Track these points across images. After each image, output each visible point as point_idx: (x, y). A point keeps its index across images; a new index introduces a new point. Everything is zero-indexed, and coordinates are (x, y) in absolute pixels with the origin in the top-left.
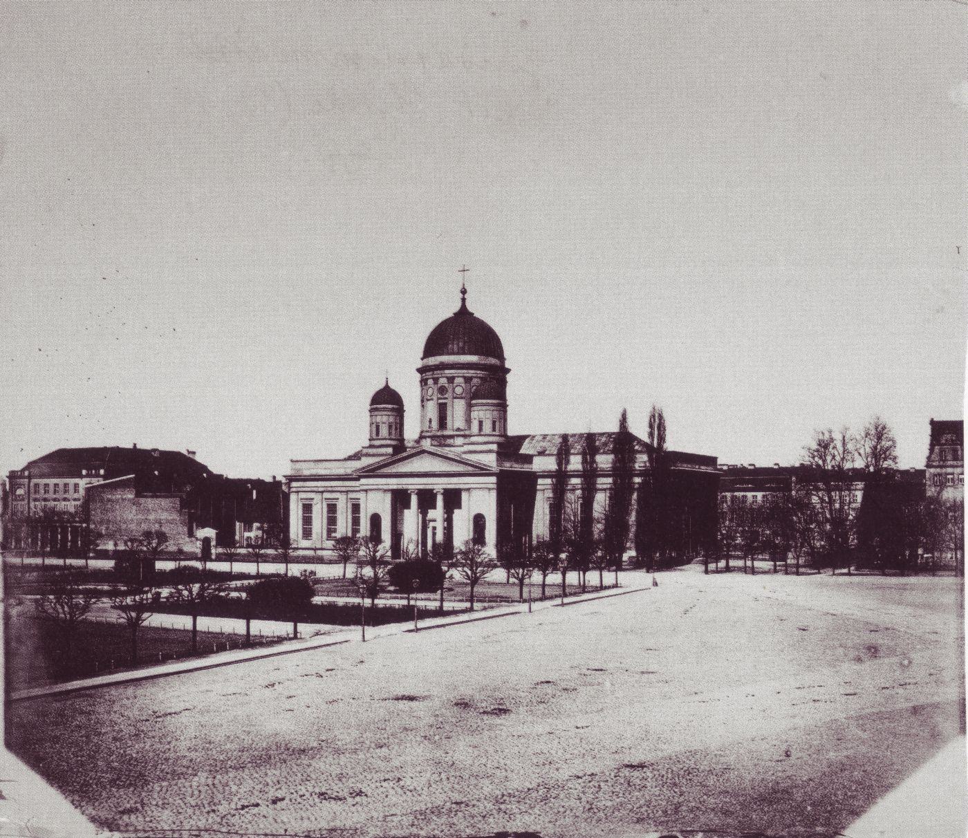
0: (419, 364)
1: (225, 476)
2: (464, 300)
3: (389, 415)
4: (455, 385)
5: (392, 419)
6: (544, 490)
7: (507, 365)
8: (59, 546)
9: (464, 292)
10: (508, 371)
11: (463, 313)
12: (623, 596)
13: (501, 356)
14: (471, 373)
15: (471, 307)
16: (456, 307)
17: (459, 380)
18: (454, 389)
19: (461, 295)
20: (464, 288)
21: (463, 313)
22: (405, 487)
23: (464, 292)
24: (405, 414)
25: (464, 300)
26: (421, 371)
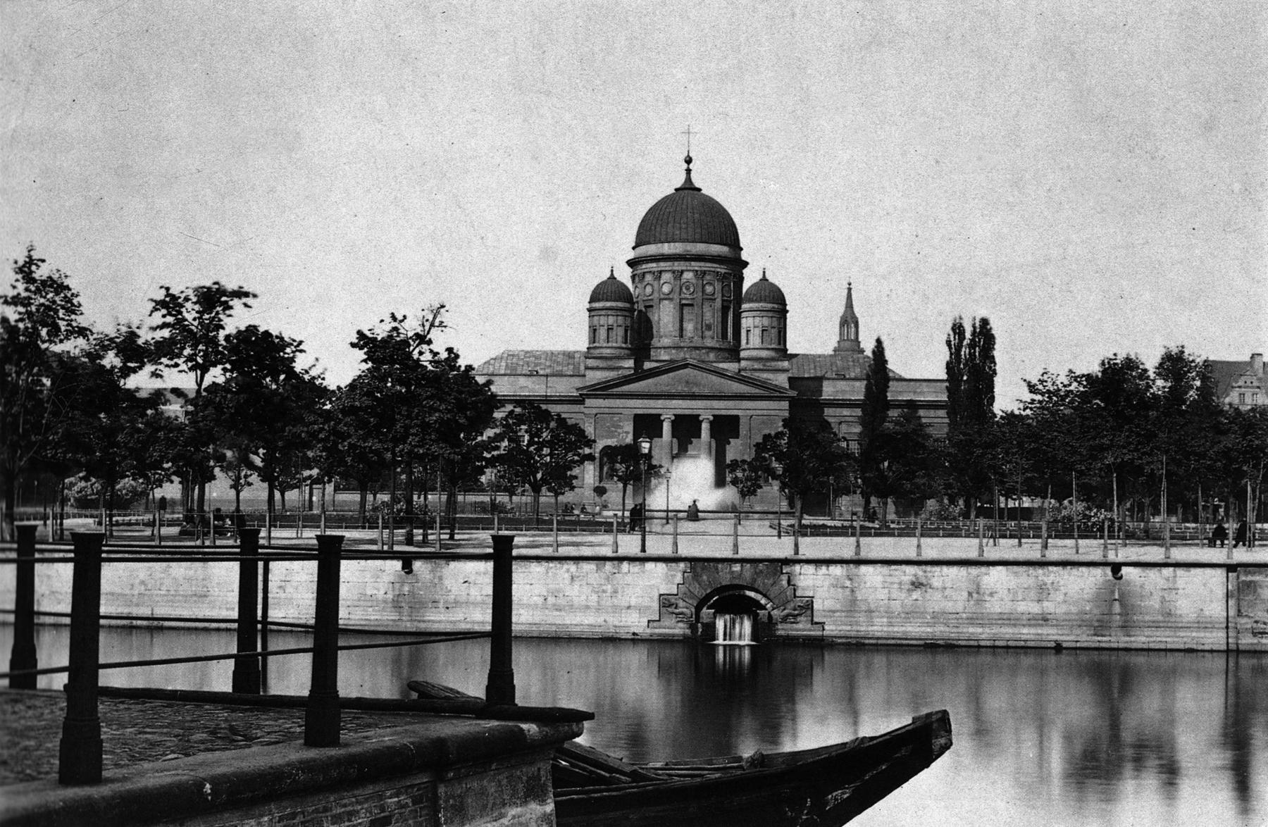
0: (631, 255)
1: (261, 329)
2: (688, 171)
3: (626, 316)
4: (662, 282)
5: (766, 322)
6: (547, 376)
7: (745, 256)
8: (226, 352)
9: (689, 161)
10: (745, 264)
11: (688, 187)
12: (1163, 654)
13: (736, 245)
14: (678, 266)
15: (697, 182)
16: (679, 181)
17: (688, 276)
18: (703, 286)
19: (685, 166)
20: (688, 156)
21: (688, 187)
22: (696, 412)
23: (689, 161)
24: (790, 318)
25: (688, 171)
26: (589, 310)
